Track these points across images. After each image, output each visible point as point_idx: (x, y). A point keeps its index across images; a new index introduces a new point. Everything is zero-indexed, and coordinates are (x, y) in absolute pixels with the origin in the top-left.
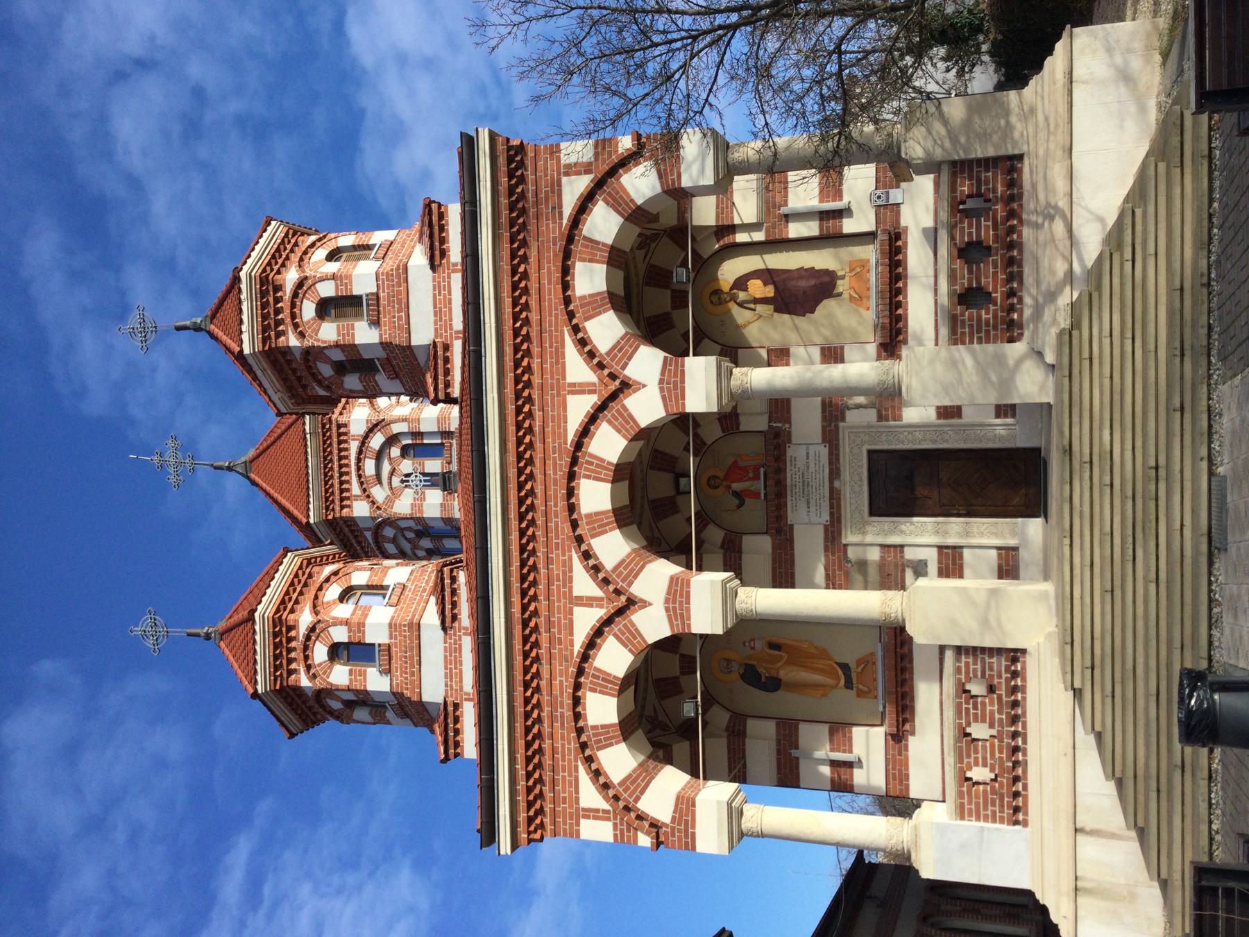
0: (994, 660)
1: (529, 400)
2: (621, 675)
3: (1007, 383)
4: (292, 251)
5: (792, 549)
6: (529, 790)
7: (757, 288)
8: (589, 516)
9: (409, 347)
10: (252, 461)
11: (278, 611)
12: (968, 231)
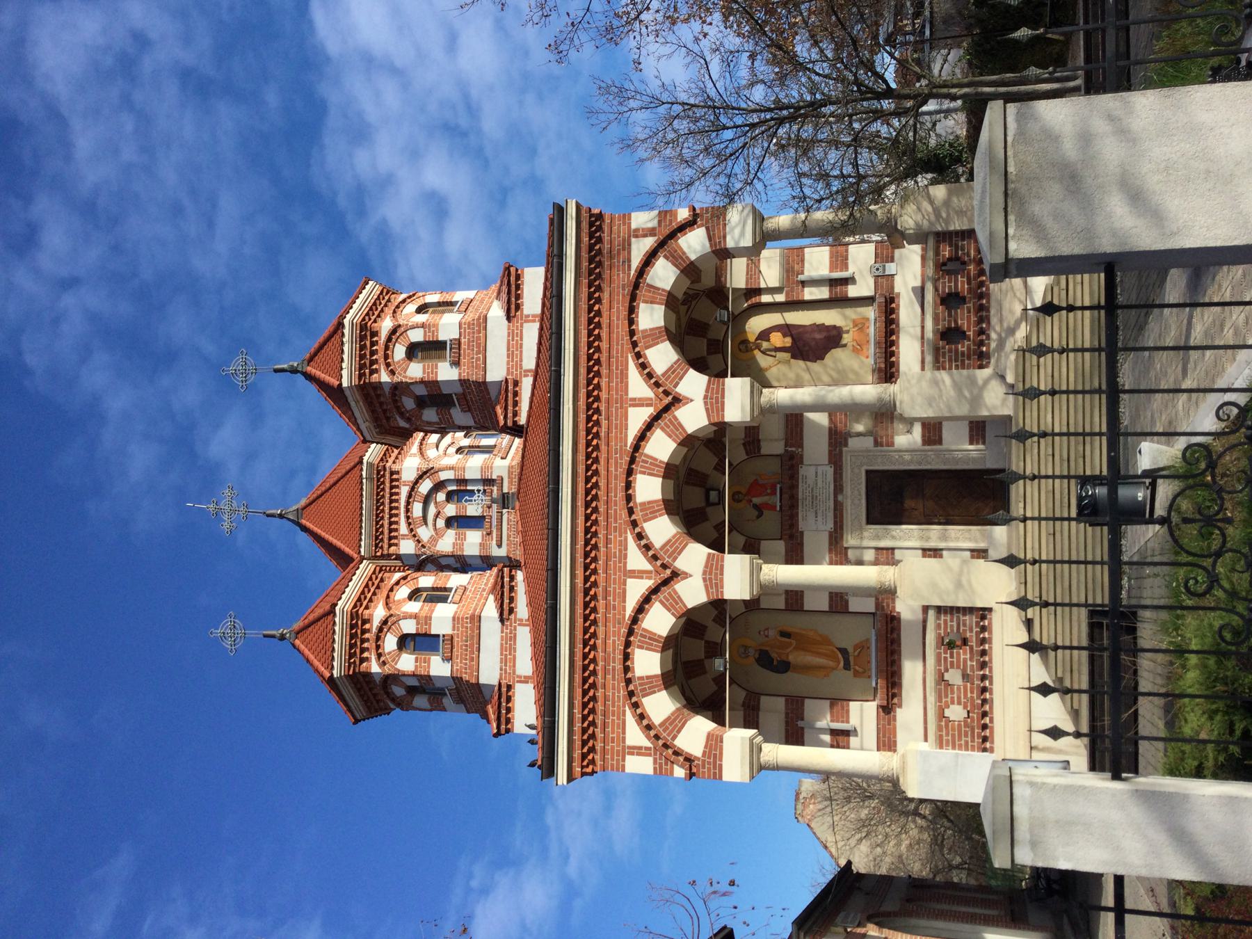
0: (967, 618)
1: (598, 411)
2: (664, 634)
3: (976, 400)
4: (386, 305)
5: (802, 551)
6: (584, 731)
7: (777, 339)
8: (643, 504)
9: (485, 383)
10: (303, 509)
11: (355, 606)
12: (947, 286)
